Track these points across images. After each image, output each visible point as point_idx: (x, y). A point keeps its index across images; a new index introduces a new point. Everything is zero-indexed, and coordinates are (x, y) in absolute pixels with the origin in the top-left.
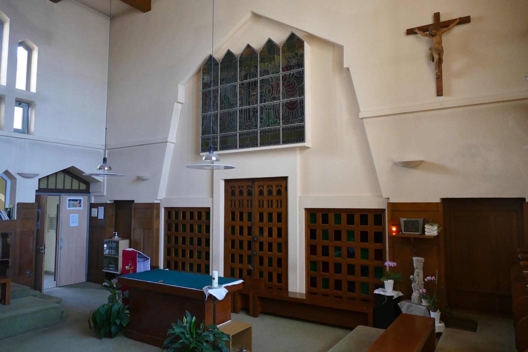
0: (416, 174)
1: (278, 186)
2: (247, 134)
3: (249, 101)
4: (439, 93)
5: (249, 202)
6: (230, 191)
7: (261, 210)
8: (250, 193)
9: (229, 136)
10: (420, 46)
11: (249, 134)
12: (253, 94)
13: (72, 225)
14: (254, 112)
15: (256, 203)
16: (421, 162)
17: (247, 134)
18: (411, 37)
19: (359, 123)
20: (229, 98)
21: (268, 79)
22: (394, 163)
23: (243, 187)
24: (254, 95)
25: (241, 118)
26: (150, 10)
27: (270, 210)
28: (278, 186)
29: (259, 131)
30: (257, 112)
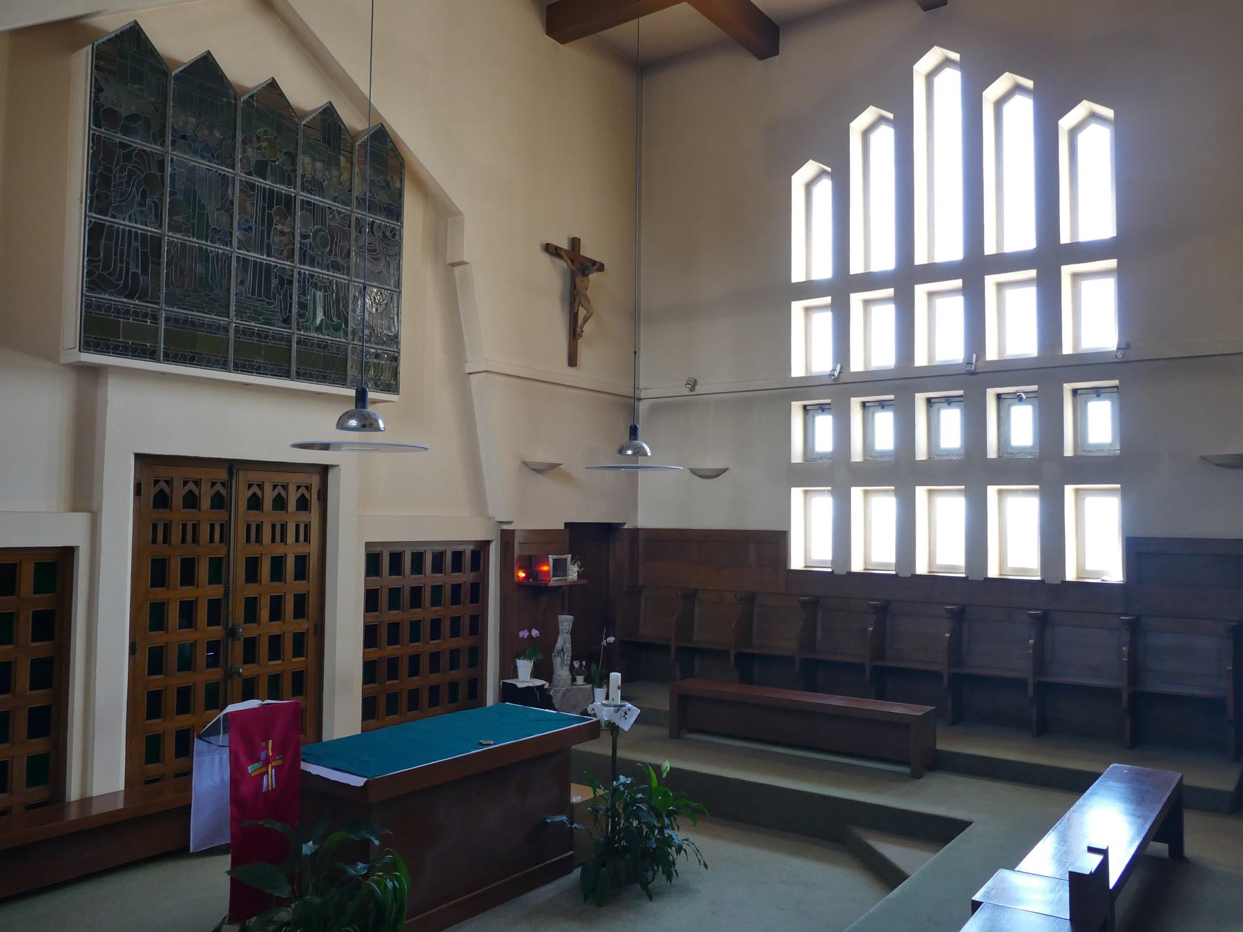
0: (546, 484)
1: (306, 489)
2: (259, 335)
3: (269, 245)
4: (572, 361)
5: (278, 529)
6: (150, 491)
7: (253, 550)
8: (219, 502)
9: (202, 325)
10: (552, 275)
11: (267, 337)
12: (279, 227)
13: (570, 617)
14: (282, 279)
15: (238, 533)
16: (554, 466)
17: (259, 335)
18: (546, 257)
19: (461, 377)
20: (202, 207)
21: (323, 209)
22: (525, 463)
23: (307, 487)
24: (282, 233)
25: (242, 283)
26: (777, 53)
27: (279, 550)
28: (306, 489)
29: (295, 339)
30: (290, 283)
